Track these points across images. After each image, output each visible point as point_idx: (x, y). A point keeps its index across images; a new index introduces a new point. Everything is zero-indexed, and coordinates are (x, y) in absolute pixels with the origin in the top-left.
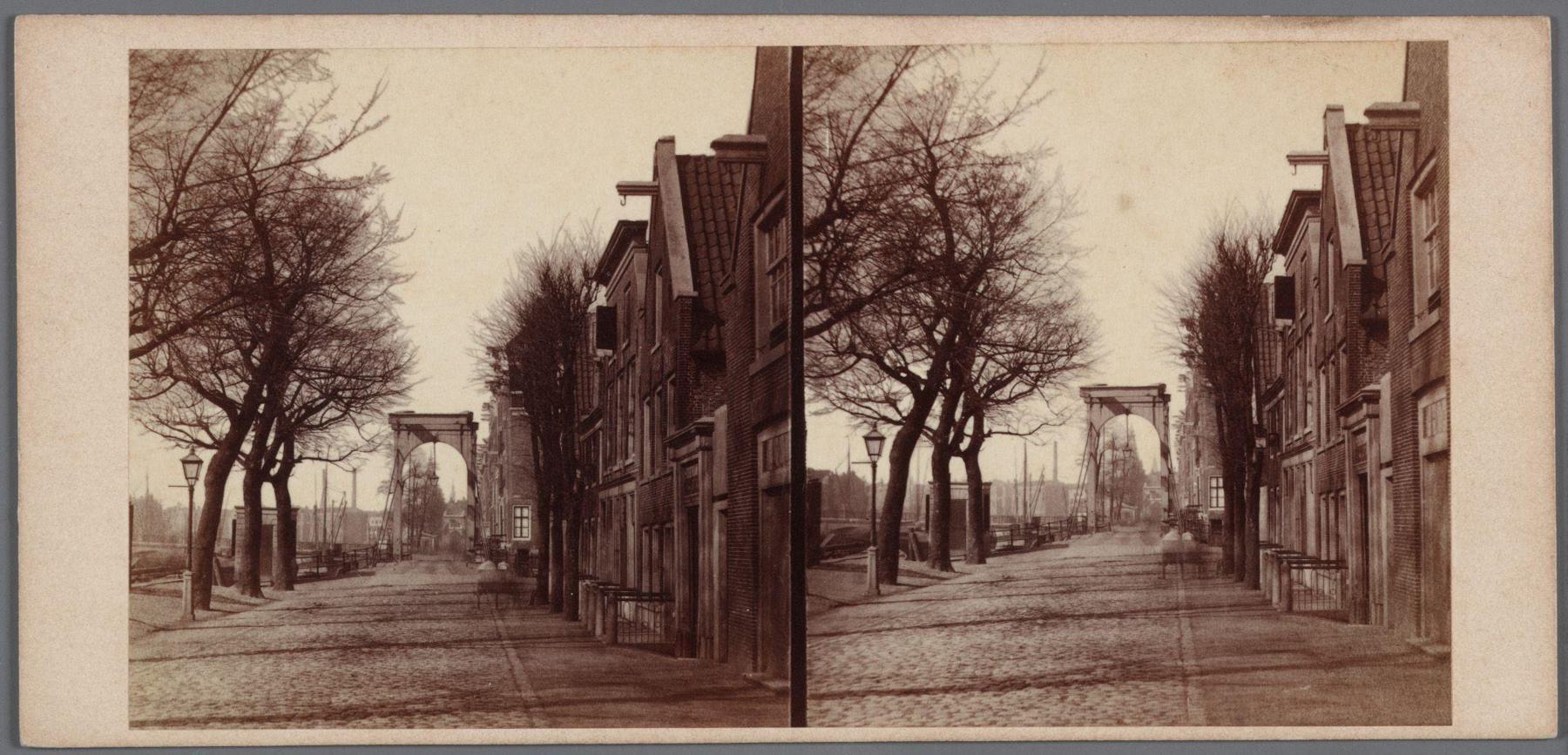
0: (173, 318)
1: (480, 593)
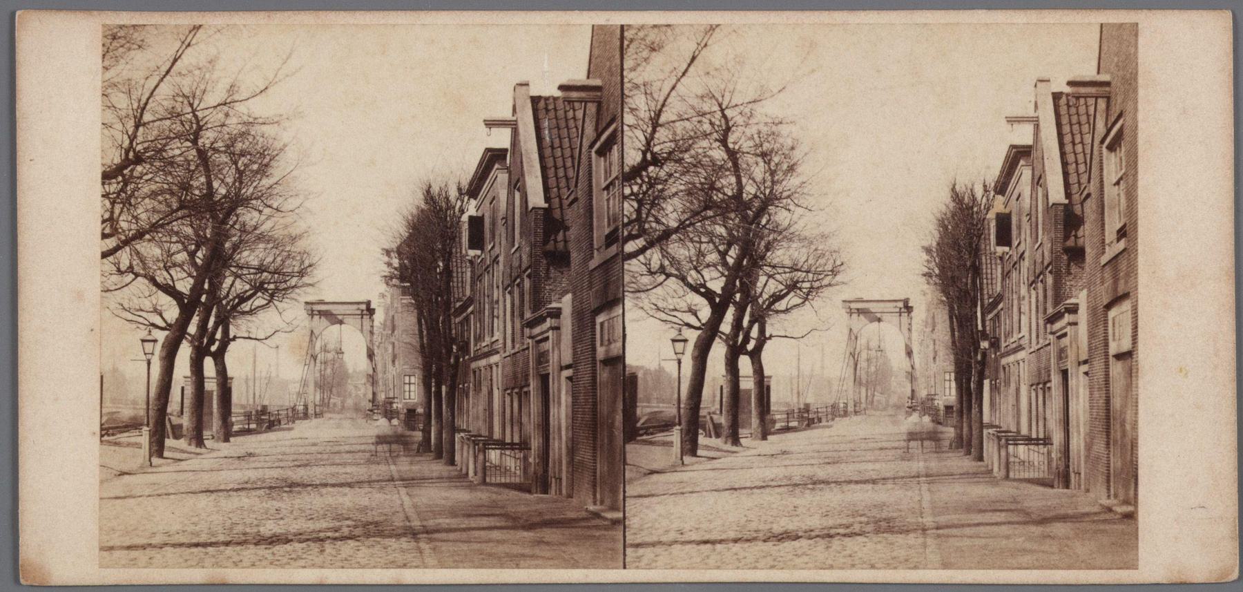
0: (134, 226)
1: (377, 443)
